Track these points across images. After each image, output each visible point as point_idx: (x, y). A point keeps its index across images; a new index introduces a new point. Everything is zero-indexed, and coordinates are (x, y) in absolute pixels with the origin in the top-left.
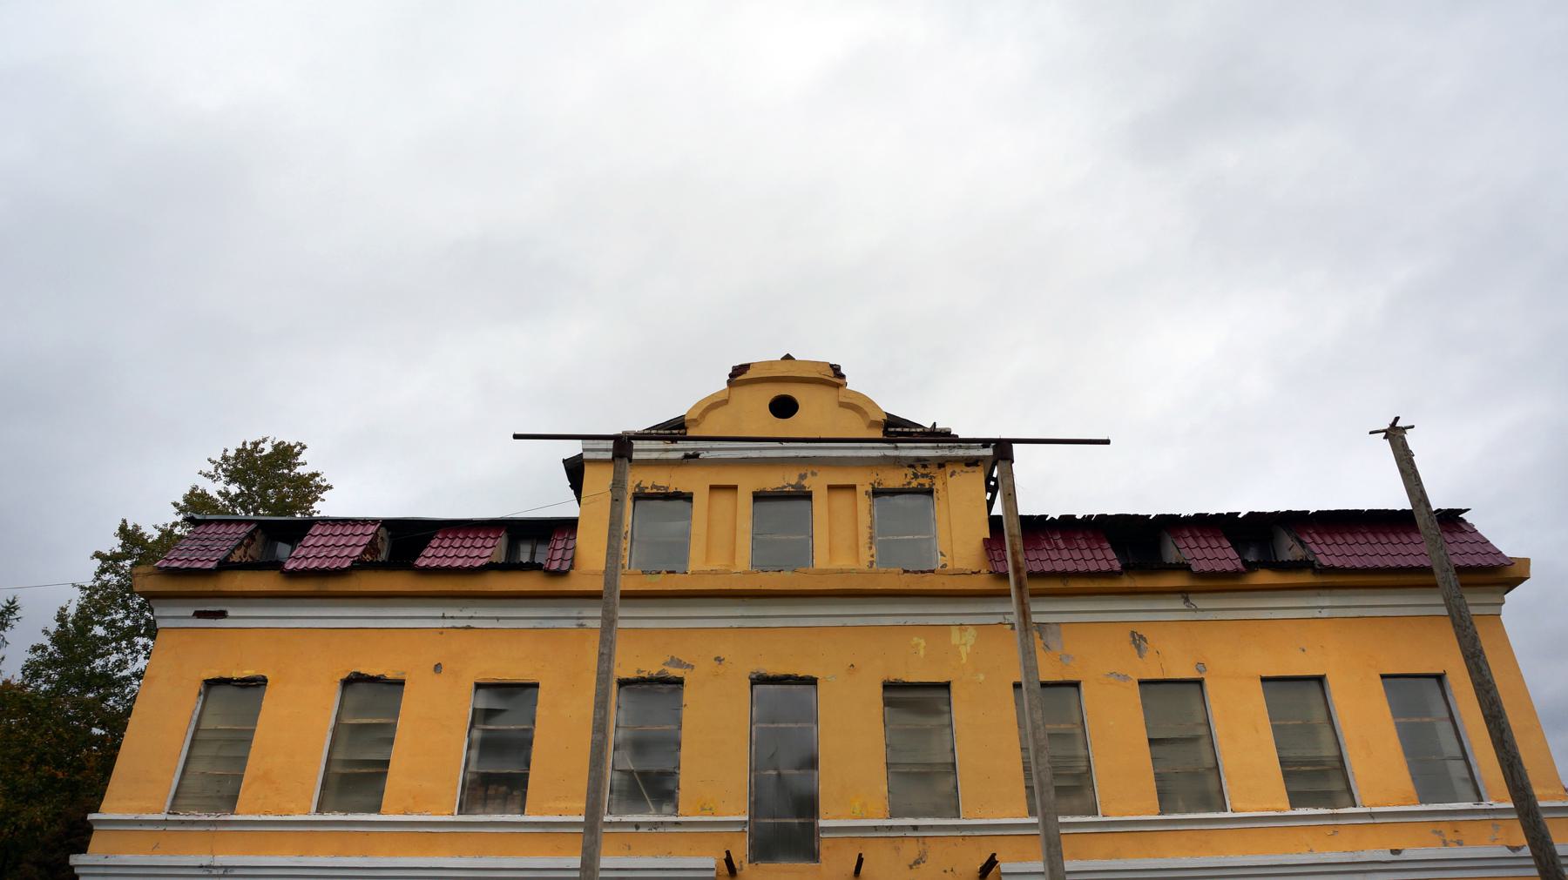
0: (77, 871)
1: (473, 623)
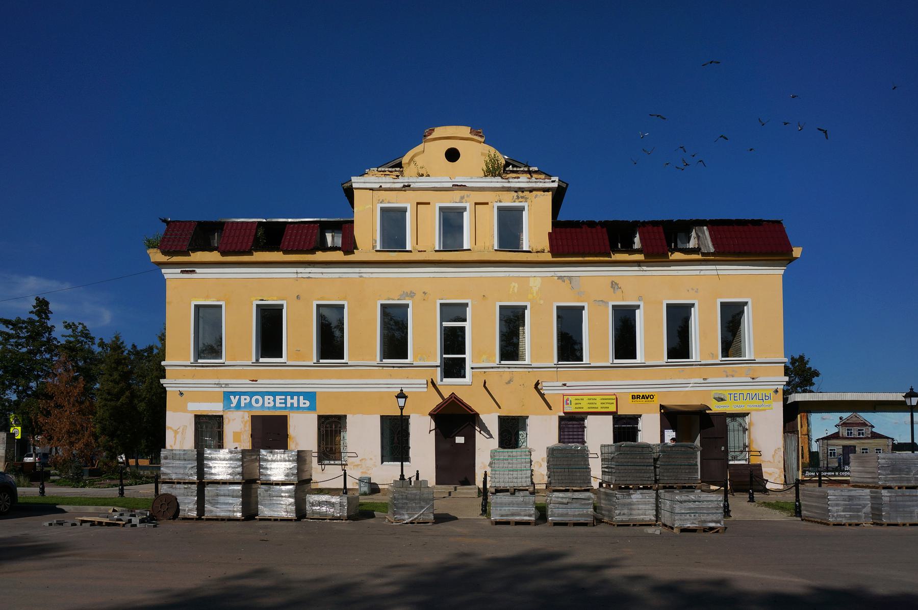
0: (164, 385)
1: (310, 275)
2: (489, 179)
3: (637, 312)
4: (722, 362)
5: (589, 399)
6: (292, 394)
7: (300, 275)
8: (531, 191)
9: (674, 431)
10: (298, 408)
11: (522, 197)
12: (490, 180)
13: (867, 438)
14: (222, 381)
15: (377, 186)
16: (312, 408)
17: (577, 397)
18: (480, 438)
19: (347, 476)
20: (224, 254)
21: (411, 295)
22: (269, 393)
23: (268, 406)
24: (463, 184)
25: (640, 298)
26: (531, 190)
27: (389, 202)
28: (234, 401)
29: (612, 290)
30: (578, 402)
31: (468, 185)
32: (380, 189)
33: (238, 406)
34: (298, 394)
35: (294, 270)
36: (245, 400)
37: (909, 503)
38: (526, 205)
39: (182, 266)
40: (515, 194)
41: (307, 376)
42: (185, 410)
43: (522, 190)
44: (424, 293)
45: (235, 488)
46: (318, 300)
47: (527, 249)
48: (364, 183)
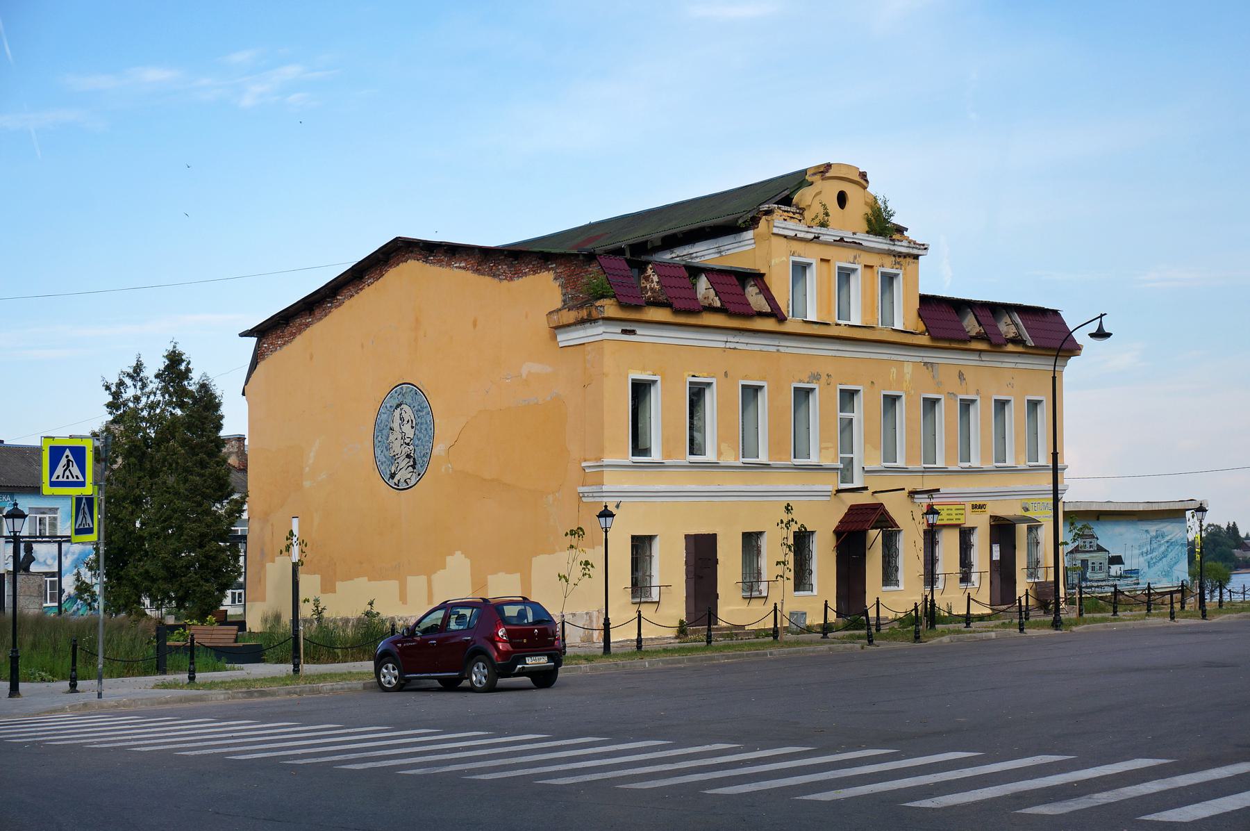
1: (738, 346)
2: (872, 238)
4: (691, 464)
5: (948, 509)
7: (728, 345)
8: (905, 257)
9: (462, 553)
11: (899, 263)
12: (880, 240)
13: (1094, 551)
15: (792, 234)
17: (949, 507)
19: (880, 605)
20: (677, 312)
21: (816, 377)
24: (860, 242)
27: (799, 256)
29: (959, 380)
30: (949, 512)
31: (864, 243)
38: (900, 272)
39: (623, 323)
40: (893, 259)
44: (828, 375)
45: (302, 644)
46: (745, 378)
47: (901, 328)
48: (784, 228)
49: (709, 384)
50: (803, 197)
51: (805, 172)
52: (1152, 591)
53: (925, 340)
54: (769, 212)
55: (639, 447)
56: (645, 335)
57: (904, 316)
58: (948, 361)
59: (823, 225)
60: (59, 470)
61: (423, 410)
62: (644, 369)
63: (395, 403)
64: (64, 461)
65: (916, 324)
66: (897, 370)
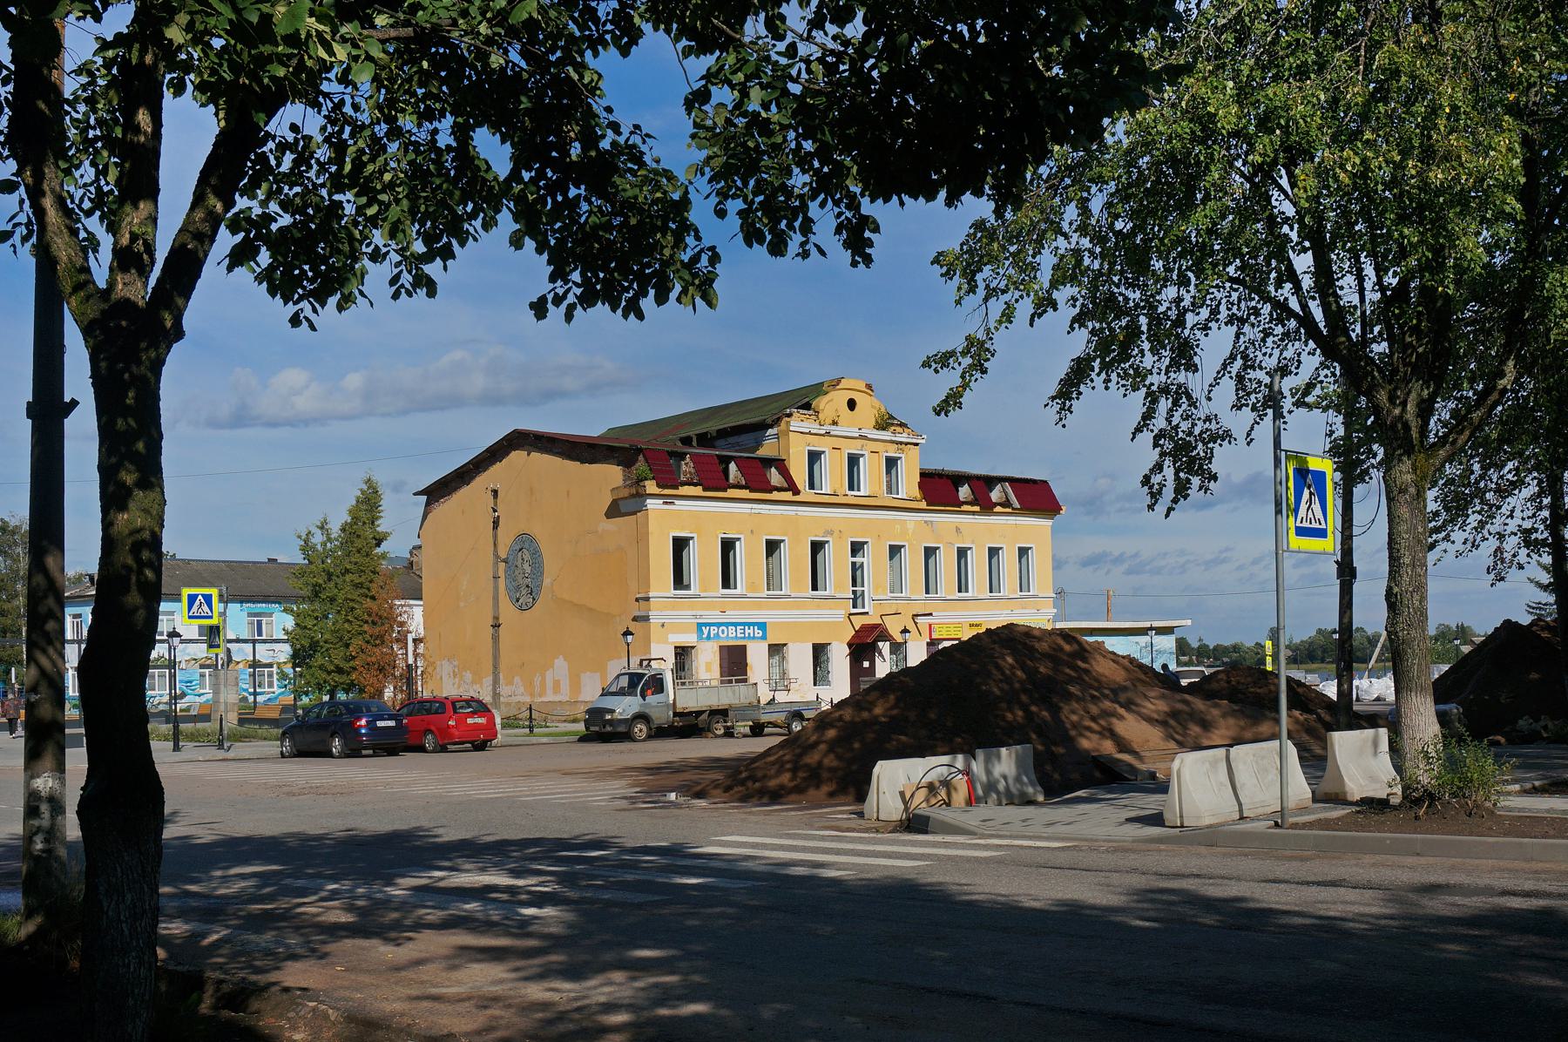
2: (875, 432)
3: (738, 543)
6: (749, 624)
10: (754, 638)
14: (699, 613)
16: (764, 637)
18: (878, 660)
21: (831, 533)
22: (740, 624)
23: (731, 637)
25: (973, 542)
26: (907, 444)
28: (706, 631)
32: (810, 433)
33: (709, 637)
34: (754, 624)
35: (750, 506)
36: (714, 630)
37: (1145, 905)
41: (759, 607)
42: (666, 642)
43: (901, 443)
49: (739, 539)
50: (822, 403)
51: (822, 384)
52: (527, 723)
53: (923, 505)
54: (790, 415)
55: (727, 582)
56: (680, 504)
57: (908, 484)
58: (945, 520)
59: (835, 423)
60: (195, 608)
61: (536, 555)
62: (683, 529)
63: (518, 548)
64: (197, 602)
65: (916, 492)
66: (1386, 453)
